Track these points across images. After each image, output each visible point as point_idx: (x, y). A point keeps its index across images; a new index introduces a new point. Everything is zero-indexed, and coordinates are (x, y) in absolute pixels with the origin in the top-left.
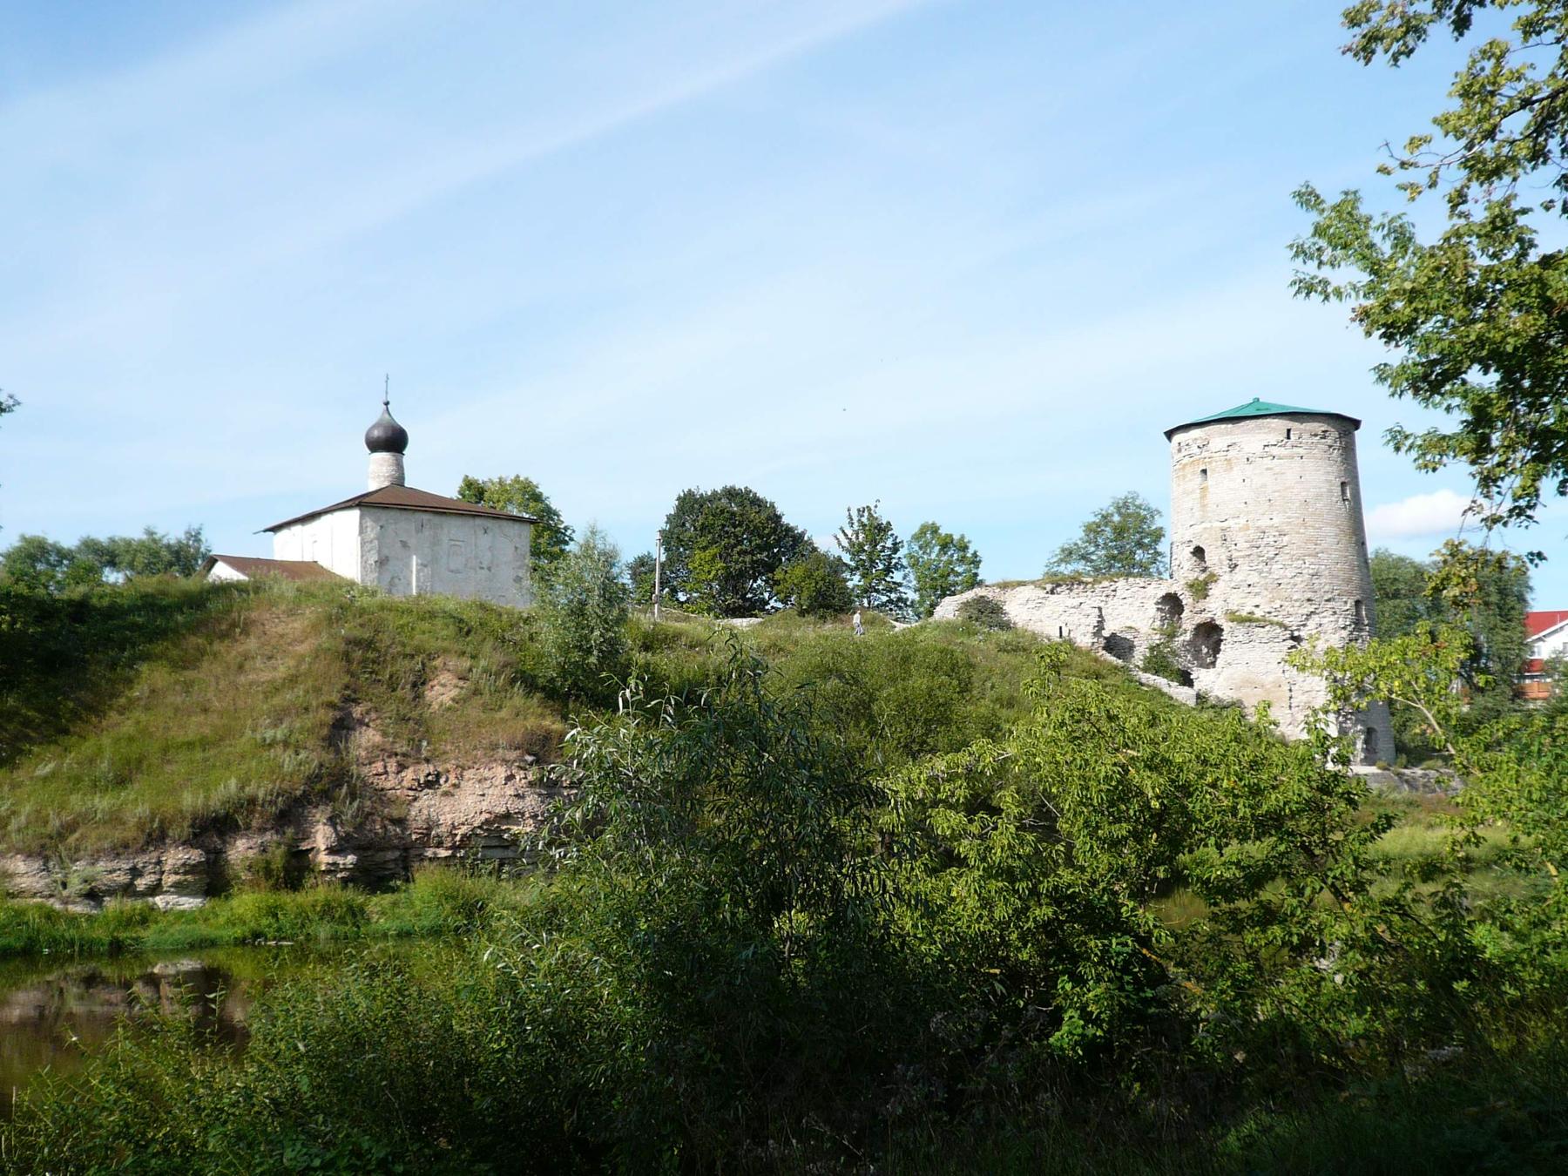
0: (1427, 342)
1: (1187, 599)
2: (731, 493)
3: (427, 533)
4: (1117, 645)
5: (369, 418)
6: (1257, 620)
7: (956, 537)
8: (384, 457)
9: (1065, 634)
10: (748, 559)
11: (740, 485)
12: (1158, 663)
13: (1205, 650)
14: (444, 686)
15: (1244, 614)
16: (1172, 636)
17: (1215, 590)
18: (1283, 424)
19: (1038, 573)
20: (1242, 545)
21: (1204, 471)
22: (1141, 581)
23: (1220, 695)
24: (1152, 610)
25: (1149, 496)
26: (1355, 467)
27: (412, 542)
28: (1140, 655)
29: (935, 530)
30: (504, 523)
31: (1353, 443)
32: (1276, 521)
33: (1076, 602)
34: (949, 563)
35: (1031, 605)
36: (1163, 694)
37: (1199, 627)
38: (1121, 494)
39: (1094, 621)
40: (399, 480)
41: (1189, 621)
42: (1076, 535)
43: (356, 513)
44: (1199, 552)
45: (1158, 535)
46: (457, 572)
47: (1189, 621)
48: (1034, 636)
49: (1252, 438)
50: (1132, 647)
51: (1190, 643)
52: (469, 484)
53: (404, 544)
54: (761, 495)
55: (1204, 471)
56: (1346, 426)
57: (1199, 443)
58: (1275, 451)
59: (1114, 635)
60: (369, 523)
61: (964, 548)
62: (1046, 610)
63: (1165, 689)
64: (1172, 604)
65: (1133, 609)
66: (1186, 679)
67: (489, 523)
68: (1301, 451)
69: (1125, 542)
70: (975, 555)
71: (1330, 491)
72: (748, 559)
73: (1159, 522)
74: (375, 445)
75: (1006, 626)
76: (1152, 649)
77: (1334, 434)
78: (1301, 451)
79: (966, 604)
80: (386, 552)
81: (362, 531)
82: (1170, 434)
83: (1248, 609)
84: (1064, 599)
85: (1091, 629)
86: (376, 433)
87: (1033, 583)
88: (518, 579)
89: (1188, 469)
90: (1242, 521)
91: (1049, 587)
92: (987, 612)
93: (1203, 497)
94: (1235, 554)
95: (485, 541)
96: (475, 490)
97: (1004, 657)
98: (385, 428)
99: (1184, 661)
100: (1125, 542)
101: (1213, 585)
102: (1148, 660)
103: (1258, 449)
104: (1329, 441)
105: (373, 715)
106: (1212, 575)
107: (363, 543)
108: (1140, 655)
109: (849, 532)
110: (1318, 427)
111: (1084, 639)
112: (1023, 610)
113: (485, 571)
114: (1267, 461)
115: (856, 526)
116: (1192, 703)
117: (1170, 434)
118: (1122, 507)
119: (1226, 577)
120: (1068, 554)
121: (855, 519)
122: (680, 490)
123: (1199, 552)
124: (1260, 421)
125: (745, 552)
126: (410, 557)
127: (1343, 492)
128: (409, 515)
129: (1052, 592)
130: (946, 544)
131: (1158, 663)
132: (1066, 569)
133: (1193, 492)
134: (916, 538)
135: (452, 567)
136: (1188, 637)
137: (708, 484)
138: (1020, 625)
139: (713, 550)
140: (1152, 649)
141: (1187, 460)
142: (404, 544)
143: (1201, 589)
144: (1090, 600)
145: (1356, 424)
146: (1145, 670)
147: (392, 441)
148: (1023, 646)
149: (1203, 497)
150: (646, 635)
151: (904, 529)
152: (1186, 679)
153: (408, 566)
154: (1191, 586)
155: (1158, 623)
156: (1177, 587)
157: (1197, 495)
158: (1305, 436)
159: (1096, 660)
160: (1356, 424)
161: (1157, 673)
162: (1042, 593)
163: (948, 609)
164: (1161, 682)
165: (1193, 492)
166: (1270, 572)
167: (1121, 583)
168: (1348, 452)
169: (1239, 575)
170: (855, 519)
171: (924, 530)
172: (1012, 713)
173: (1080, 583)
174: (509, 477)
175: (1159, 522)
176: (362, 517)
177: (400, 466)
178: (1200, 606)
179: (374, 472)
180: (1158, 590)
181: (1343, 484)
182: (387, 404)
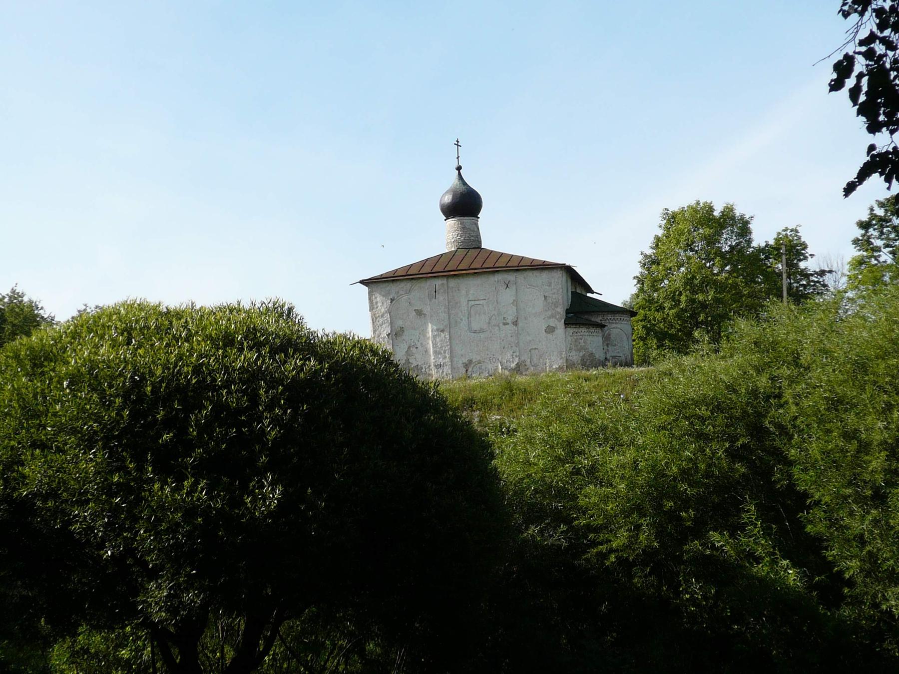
0: (732, 470)
3: (441, 297)
5: (443, 189)
27: (427, 310)
30: (530, 274)
40: (471, 242)
46: (481, 331)
53: (419, 313)
60: (379, 298)
67: (511, 277)
74: (450, 211)
80: (400, 323)
88: (550, 330)
95: (507, 296)
113: (510, 328)
122: (287, 298)
126: (426, 324)
135: (475, 326)
142: (419, 313)
147: (464, 205)
153: (424, 332)
182: (459, 168)
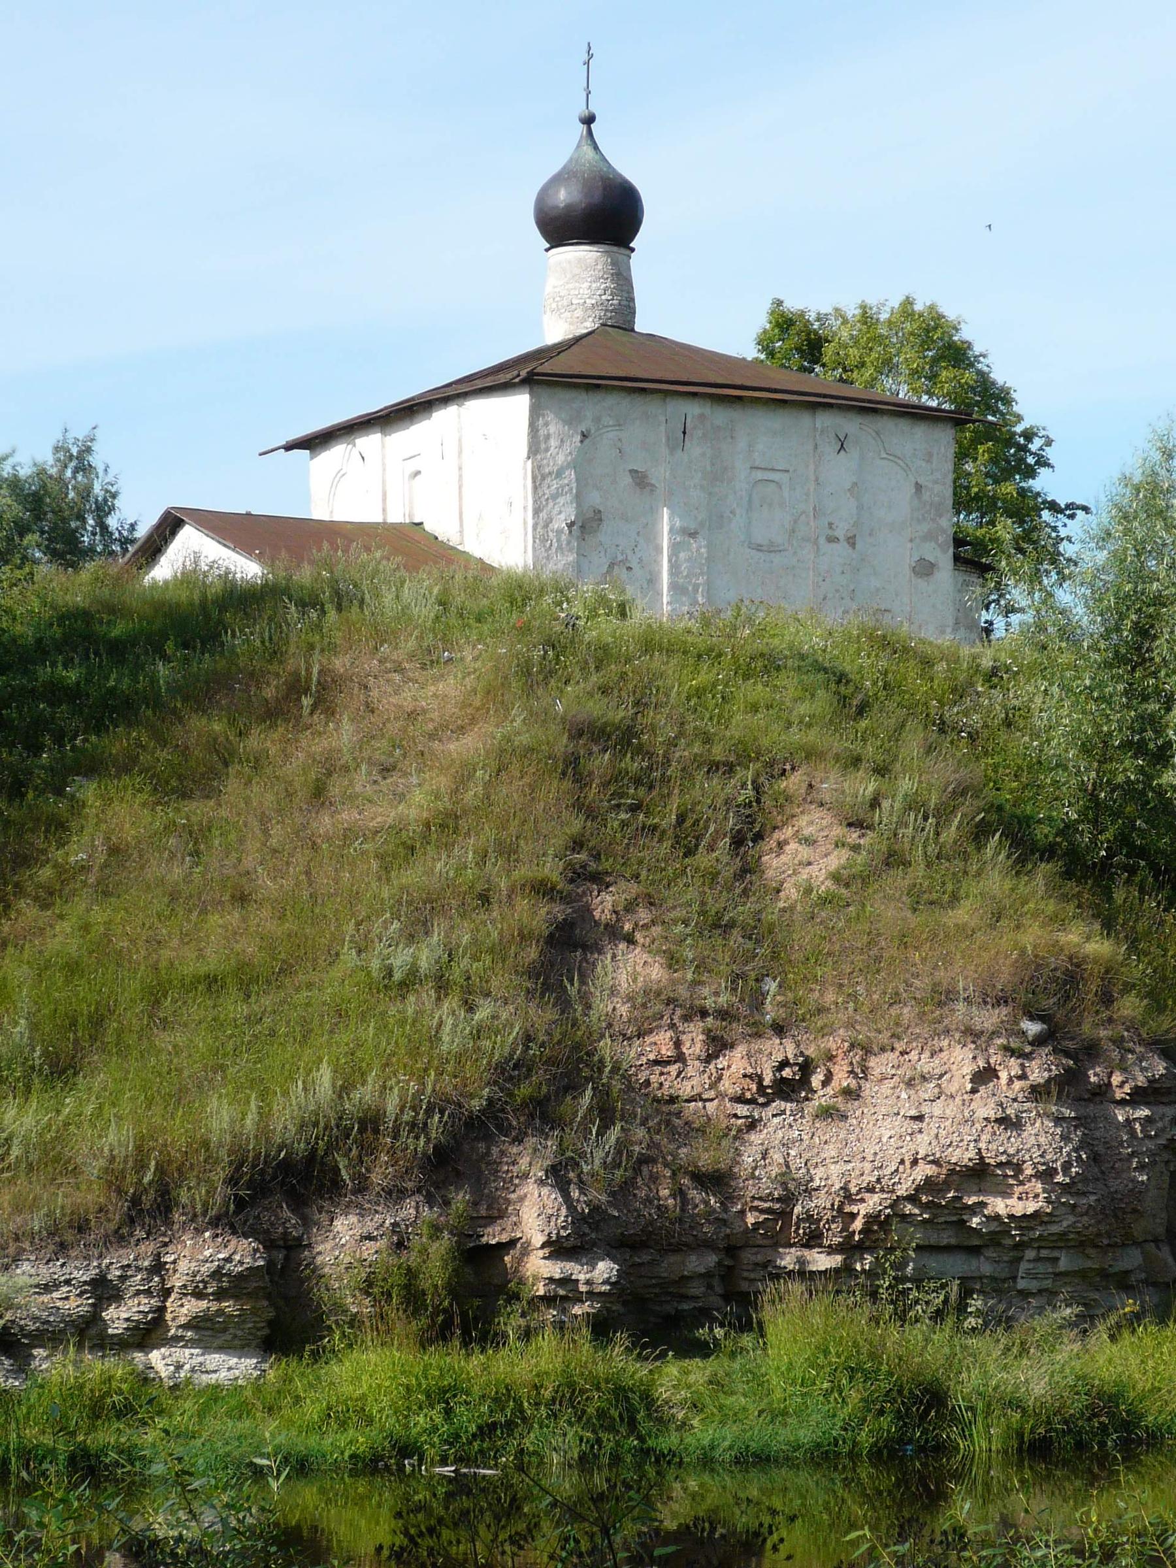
5: (543, 159)
8: (582, 258)
40: (620, 315)
43: (519, 403)
60: (553, 426)
74: (559, 228)
81: (536, 447)
86: (563, 197)
105: (644, 915)
107: (539, 479)
174: (886, 298)
176: (535, 412)
177: (622, 281)
179: (559, 296)
182: (589, 120)
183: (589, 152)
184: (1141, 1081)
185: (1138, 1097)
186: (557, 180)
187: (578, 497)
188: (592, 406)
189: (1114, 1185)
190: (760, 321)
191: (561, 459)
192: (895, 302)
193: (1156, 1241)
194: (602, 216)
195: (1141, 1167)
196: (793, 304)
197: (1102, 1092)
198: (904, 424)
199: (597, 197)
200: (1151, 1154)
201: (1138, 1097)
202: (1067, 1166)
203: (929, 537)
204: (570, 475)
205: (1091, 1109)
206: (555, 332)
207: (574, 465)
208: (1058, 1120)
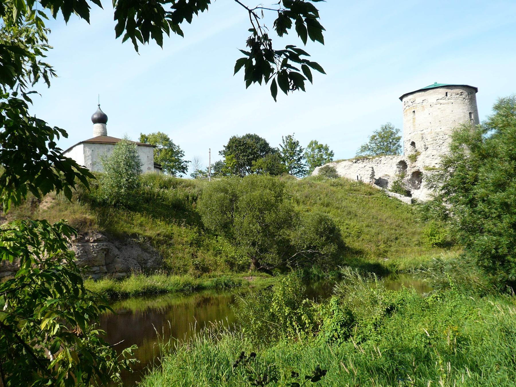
1: (408, 163)
2: (249, 136)
4: (380, 182)
5: (93, 112)
6: (437, 169)
7: (324, 145)
8: (98, 125)
9: (359, 178)
10: (246, 158)
11: (252, 133)
12: (397, 188)
13: (417, 182)
14: (47, 202)
15: (431, 167)
16: (402, 177)
17: (420, 158)
18: (444, 90)
19: (353, 156)
20: (430, 140)
21: (414, 112)
22: (391, 157)
23: (422, 200)
24: (395, 168)
25: (395, 125)
26: (476, 106)
28: (390, 186)
29: (316, 143)
30: (143, 147)
31: (475, 97)
32: (443, 129)
33: (363, 166)
34: (321, 155)
35: (346, 168)
36: (397, 199)
37: (414, 173)
38: (384, 124)
39: (370, 172)
40: (105, 134)
41: (410, 171)
42: (367, 141)
43: (82, 145)
44: (413, 144)
45: (399, 139)
47: (410, 171)
48: (347, 180)
49: (432, 97)
50: (387, 183)
51: (410, 180)
52: (142, 136)
54: (260, 137)
55: (414, 112)
56: (472, 91)
57: (412, 101)
58: (441, 101)
59: (380, 178)
60: (87, 149)
61: (327, 149)
62: (352, 170)
63: (399, 198)
64: (403, 164)
65: (387, 168)
66: (408, 194)
68: (452, 101)
69: (386, 142)
70: (332, 152)
71: (465, 116)
72: (246, 158)
73: (399, 134)
74: (95, 121)
75: (336, 176)
76: (395, 183)
77: (465, 93)
78: (452, 101)
79: (322, 169)
81: (85, 152)
82: (401, 98)
83: (433, 165)
84: (360, 164)
85: (369, 176)
86: (95, 116)
87: (349, 160)
89: (408, 111)
90: (429, 130)
91: (354, 161)
92: (331, 172)
93: (414, 122)
94: (427, 143)
96: (144, 138)
97: (332, 188)
98: (98, 114)
99: (408, 187)
100: (386, 142)
101: (418, 157)
102: (393, 187)
103: (435, 101)
104: (464, 96)
105: (9, 215)
106: (419, 152)
107: (85, 157)
108: (390, 186)
109: (283, 146)
110: (459, 91)
111: (366, 180)
112: (342, 170)
114: (438, 106)
115: (285, 144)
116: (410, 203)
117: (401, 98)
118: (385, 129)
119: (424, 153)
120: (365, 148)
121: (285, 140)
123: (413, 144)
124: (435, 90)
125: (245, 156)
127: (470, 117)
128: (104, 146)
129: (356, 162)
130: (320, 148)
131: (397, 188)
132: (363, 154)
133: (410, 120)
134: (309, 146)
136: (409, 177)
137: (240, 134)
138: (342, 176)
139: (232, 155)
140: (395, 183)
141: (407, 108)
143: (414, 158)
144: (368, 165)
145: (475, 90)
146: (392, 191)
148: (341, 183)
149: (414, 122)
150: (165, 182)
151: (304, 144)
152: (408, 194)
154: (410, 157)
155: (398, 173)
156: (405, 158)
157: (412, 121)
158: (453, 95)
159: (371, 188)
160: (475, 90)
161: (396, 192)
162: (350, 163)
163: (316, 172)
164: (397, 195)
165: (410, 120)
166: (441, 150)
167: (383, 158)
168: (472, 101)
169: (429, 152)
170: (285, 140)
171: (311, 143)
172: (328, 209)
173: (367, 159)
174: (156, 132)
175: (399, 134)
176: (84, 147)
177: (105, 129)
178: (413, 165)
179: (95, 131)
180: (397, 159)
181: (470, 113)
182: (99, 105)
183: (99, 110)
184: (95, 239)
185: (94, 241)
186: (94, 114)
187: (92, 160)
188: (93, 146)
189: (89, 256)
190: (140, 136)
191: (89, 154)
192: (157, 132)
193: (102, 265)
194: (102, 119)
195: (95, 253)
196: (143, 134)
197: (88, 241)
198: (145, 147)
199: (99, 116)
200: (97, 251)
201: (94, 241)
202: (78, 254)
203: (150, 164)
204: (90, 156)
205: (85, 244)
206: (95, 136)
207: (91, 155)
208: (77, 246)
